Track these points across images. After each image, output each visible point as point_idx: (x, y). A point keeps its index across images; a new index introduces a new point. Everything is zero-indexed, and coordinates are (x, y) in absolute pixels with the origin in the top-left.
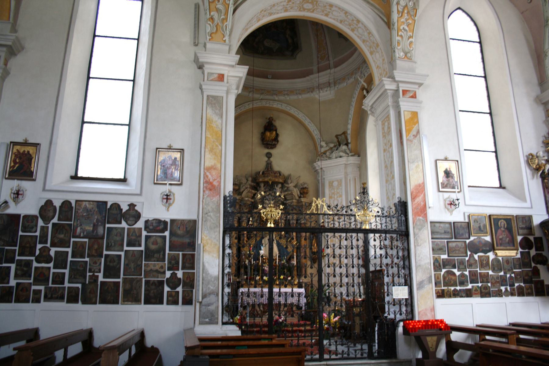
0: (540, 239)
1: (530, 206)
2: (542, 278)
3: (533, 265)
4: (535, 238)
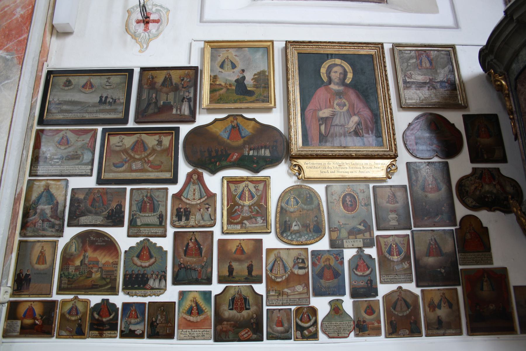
0: (493, 119)
1: (450, 22)
2: (497, 262)
3: (461, 211)
4: (467, 119)
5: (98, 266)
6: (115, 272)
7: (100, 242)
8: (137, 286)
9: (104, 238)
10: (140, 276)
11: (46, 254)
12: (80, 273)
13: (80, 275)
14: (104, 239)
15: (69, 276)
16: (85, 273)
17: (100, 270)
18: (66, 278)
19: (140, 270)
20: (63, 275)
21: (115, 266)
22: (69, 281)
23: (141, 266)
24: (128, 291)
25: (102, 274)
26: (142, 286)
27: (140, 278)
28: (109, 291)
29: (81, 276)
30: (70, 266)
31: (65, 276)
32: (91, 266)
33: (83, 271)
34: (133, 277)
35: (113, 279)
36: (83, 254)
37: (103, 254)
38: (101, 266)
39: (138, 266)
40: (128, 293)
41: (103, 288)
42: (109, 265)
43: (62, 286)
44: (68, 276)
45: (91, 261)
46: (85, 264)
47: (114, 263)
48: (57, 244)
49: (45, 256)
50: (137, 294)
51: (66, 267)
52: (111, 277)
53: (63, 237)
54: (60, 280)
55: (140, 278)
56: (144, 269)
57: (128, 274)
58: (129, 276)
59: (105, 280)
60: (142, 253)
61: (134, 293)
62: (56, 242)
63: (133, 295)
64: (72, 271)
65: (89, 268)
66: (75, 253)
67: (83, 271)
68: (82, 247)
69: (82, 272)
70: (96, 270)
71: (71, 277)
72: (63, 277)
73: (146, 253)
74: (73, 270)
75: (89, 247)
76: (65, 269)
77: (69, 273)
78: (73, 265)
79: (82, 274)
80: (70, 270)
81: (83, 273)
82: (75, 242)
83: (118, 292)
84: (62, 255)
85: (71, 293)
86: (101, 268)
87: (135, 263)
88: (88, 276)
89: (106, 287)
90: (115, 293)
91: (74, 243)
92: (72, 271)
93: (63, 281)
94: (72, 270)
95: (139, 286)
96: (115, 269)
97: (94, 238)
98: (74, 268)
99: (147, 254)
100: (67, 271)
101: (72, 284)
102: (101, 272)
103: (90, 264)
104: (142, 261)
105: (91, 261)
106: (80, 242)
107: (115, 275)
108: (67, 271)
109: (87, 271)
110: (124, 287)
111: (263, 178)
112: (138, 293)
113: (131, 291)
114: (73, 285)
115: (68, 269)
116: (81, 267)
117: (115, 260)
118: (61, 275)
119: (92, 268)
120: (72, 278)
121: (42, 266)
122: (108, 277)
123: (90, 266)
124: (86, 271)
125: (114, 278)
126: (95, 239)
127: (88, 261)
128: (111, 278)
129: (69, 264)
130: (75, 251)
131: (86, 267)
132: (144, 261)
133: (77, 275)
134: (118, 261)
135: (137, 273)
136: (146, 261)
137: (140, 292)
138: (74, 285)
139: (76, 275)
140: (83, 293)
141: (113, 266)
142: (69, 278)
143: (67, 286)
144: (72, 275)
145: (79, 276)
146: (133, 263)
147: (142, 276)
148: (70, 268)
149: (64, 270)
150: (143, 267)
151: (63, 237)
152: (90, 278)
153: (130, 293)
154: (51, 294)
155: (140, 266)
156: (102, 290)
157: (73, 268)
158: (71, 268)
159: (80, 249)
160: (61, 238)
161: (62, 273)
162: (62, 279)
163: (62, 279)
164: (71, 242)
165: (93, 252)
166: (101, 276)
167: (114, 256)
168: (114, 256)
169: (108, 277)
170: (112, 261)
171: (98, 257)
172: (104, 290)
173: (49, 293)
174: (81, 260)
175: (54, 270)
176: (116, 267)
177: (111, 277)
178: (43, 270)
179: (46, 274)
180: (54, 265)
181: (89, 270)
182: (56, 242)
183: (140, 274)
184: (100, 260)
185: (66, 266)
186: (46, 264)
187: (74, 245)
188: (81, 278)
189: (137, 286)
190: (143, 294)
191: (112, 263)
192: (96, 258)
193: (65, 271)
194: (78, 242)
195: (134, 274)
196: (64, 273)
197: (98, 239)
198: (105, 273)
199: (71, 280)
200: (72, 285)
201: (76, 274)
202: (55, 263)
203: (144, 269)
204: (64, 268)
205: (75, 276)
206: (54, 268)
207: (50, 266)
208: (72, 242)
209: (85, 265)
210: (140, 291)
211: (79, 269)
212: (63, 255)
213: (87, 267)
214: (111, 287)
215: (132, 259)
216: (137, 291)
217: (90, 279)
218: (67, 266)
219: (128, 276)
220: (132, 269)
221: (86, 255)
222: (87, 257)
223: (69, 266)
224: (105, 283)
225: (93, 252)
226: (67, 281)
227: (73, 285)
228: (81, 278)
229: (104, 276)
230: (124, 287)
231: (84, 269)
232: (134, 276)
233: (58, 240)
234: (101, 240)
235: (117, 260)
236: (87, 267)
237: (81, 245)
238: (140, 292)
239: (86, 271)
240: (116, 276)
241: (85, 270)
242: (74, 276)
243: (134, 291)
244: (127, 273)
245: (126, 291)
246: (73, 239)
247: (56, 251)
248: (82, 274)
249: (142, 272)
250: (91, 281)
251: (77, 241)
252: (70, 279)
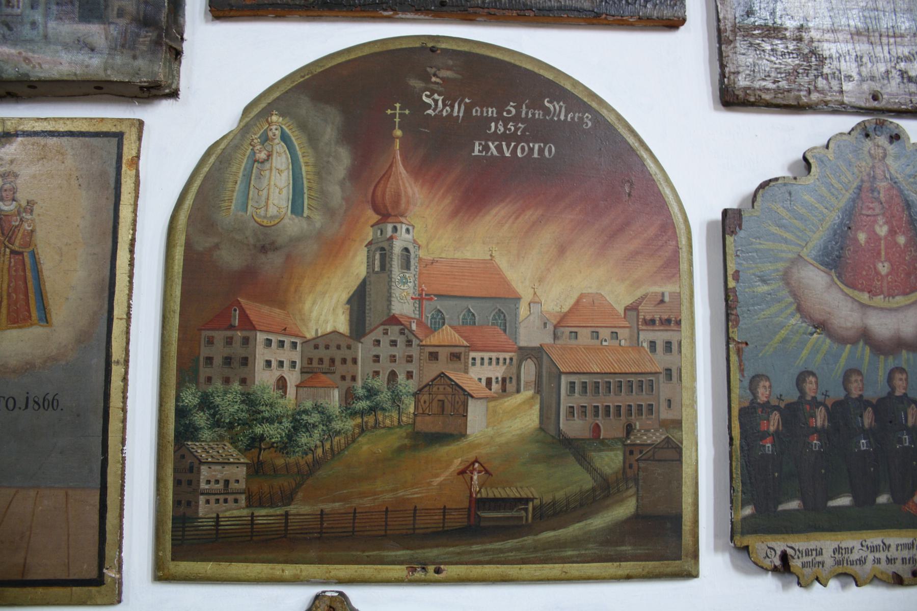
5: (515, 336)
6: (664, 390)
7: (508, 137)
8: (844, 501)
9: (536, 104)
10: (868, 419)
11: (40, 235)
12: (349, 396)
13: (354, 414)
14: (539, 114)
15: (258, 430)
16: (396, 399)
17: (528, 370)
18: (234, 442)
19: (859, 373)
20: (201, 419)
21: (660, 336)
22: (256, 469)
23: (865, 336)
24: (780, 544)
25: (548, 413)
26: (883, 499)
27: (867, 433)
28: (627, 549)
29: (363, 429)
30: (261, 337)
31: (217, 423)
32: (447, 335)
33: (380, 383)
34: (764, 435)
35: (656, 447)
36: (369, 234)
37: (547, 236)
38: (535, 344)
39: (842, 340)
40: (784, 557)
41: (574, 530)
42: (605, 333)
43: (204, 509)
44: (245, 424)
45: (440, 296)
46: (393, 320)
47: (647, 311)
48: (126, 157)
49: (33, 255)
50: (856, 569)
51: (218, 351)
52: (629, 429)
53: (174, 94)
54: (180, 457)
55: (867, 433)
56: (891, 362)
57: (767, 407)
58: (775, 417)
59: (583, 459)
60: (862, 237)
61: (827, 557)
62: (120, 136)
63: (822, 573)
64: (282, 384)
65: (434, 356)
66: (293, 226)
67: (380, 383)
68: (356, 174)
69: (371, 393)
70: (497, 372)
71: (274, 432)
72: (206, 434)
73: (892, 232)
74: (293, 378)
75: (418, 172)
76: (218, 361)
77: (250, 400)
78: (285, 331)
79: (372, 410)
80: (264, 378)
81: (384, 397)
82: (284, 138)
83: (696, 556)
84: (181, 239)
85: (289, 570)
86: (536, 354)
87: (818, 316)
88: (429, 425)
89: (599, 522)
90: (673, 566)
91: (279, 147)
92: (282, 384)
93: (205, 471)
94: (276, 373)
95: (864, 499)
96: (660, 361)
97: (449, 100)
98: (296, 356)
99: (901, 240)
100: (236, 386)
101: (288, 498)
102: (538, 389)
103: (439, 320)
104: (864, 297)
105: (440, 296)
106: (329, 133)
107: (665, 414)
108: (236, 386)
109: (412, 386)
110: (748, 511)
111: (310, 517)
112: (862, 561)
113: (799, 543)
114: (300, 509)
115: (245, 361)
116: (362, 350)
117: (657, 289)
118: (181, 412)
119: (455, 357)
120: (287, 444)
121: (14, 333)
122: (611, 428)
123: (434, 339)
124: (407, 386)
125: (656, 437)
126: (458, 111)
127: (421, 299)
128: (633, 439)
129: (247, 324)
130: (296, 207)
131: (400, 351)
132: (879, 300)
133: (328, 419)
134: (677, 297)
135: (838, 394)
136: (900, 300)
137: (874, 549)
138: (305, 509)
139: (315, 418)
140: (399, 571)
141: (646, 336)
142: (256, 442)
143: (245, 512)
144: (278, 419)
145: (350, 424)
146: (799, 309)
147: (785, 421)
148: (261, 354)
149: (204, 372)
150: (879, 347)
151: (174, 94)
152: (453, 447)
153: (795, 564)
154: (110, 574)
155: (854, 342)
156: (560, 545)
157: (287, 355)
158: (275, 355)
159: (336, 193)
160: (165, 107)
161: (190, 398)
162: (197, 448)
163: (197, 448)
164: (256, 138)
165: (455, 213)
166: (541, 429)
167: (634, 254)
168: (634, 254)
169: (611, 428)
170: (628, 301)
171: (502, 263)
172: (576, 542)
173: (94, 574)
174: (354, 285)
175: (117, 371)
176: (668, 346)
177: (629, 429)
178: (27, 368)
179: (49, 403)
180: (118, 327)
181: (433, 370)
182: (119, 136)
183: (863, 402)
184: (524, 290)
185: (219, 336)
186: (45, 318)
187: (281, 161)
188: (366, 446)
189: (844, 501)
190: (898, 568)
191: (632, 309)
192: (489, 268)
193: (218, 385)
194: (313, 140)
195: (815, 403)
196: (206, 403)
197: (491, 112)
198: (578, 400)
199: (280, 461)
200: (292, 509)
201: (316, 407)
202: (119, 311)
203: (891, 362)
204: (205, 352)
205: (309, 428)
206: (117, 352)
207: (83, 338)
208: (265, 139)
209: (394, 330)
210: (874, 539)
211: (340, 369)
212: (188, 246)
213: (414, 351)
214: (636, 517)
215: (786, 277)
216: (852, 541)
217: (444, 451)
218: (229, 341)
219: (774, 422)
220: (800, 364)
221: (398, 246)
222: (406, 265)
223: (246, 341)
224: (585, 481)
225: (455, 213)
226: (241, 472)
227: (300, 509)
228: (366, 446)
229: (574, 427)
230: (748, 511)
231: (385, 367)
232: (820, 419)
233: (141, 123)
234: (517, 119)
235: (668, 289)
236: (414, 351)
237: (343, 159)
238: (874, 549)
239: (407, 386)
240: (677, 424)
241: (393, 375)
242: (299, 425)
243: (827, 544)
244: (763, 394)
245: (759, 544)
246: (266, 113)
247: (125, 212)
248: (372, 410)
249: (876, 390)
250: (457, 464)
251: (303, 126)
252: (264, 455)
